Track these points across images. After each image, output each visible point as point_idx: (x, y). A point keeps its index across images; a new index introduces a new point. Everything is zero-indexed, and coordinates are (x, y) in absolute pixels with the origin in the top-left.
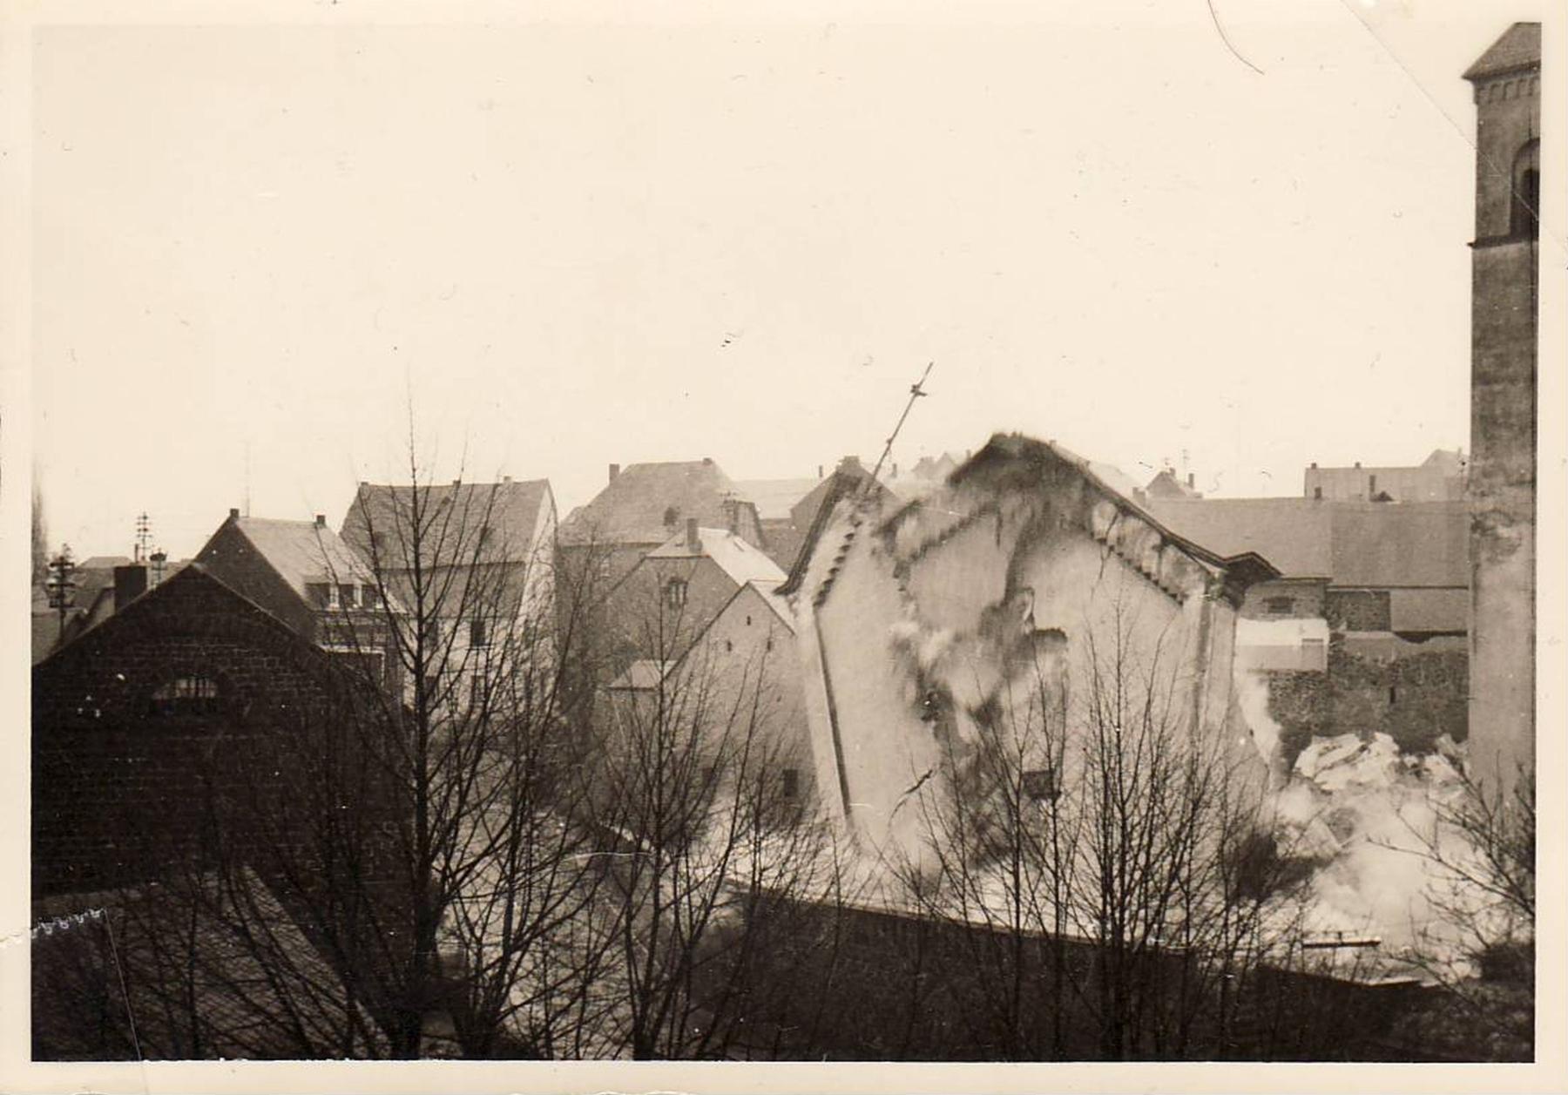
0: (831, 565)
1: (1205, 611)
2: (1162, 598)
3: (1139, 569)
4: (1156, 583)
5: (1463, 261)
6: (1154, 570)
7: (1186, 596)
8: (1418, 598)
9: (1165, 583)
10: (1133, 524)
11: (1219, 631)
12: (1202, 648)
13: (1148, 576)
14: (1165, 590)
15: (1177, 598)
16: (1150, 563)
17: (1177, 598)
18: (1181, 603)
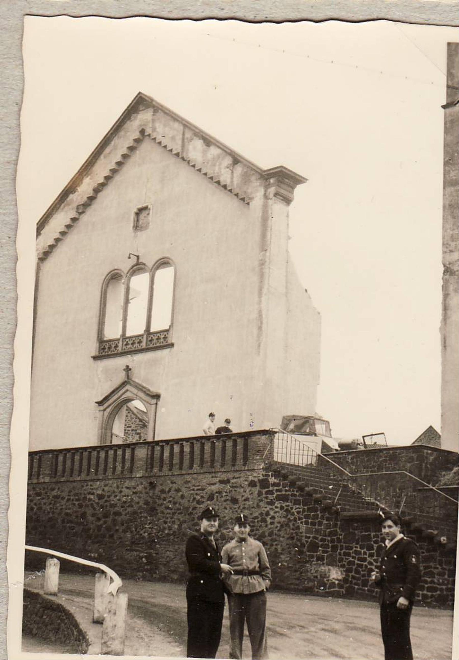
0: (57, 235)
1: (265, 207)
2: (235, 202)
3: (218, 183)
4: (230, 191)
5: (438, 117)
6: (228, 182)
7: (251, 199)
8: (363, 623)
9: (236, 191)
10: (214, 151)
11: (276, 222)
12: (264, 235)
13: (225, 187)
14: (237, 195)
15: (245, 201)
16: (225, 178)
17: (245, 201)
18: (248, 204)
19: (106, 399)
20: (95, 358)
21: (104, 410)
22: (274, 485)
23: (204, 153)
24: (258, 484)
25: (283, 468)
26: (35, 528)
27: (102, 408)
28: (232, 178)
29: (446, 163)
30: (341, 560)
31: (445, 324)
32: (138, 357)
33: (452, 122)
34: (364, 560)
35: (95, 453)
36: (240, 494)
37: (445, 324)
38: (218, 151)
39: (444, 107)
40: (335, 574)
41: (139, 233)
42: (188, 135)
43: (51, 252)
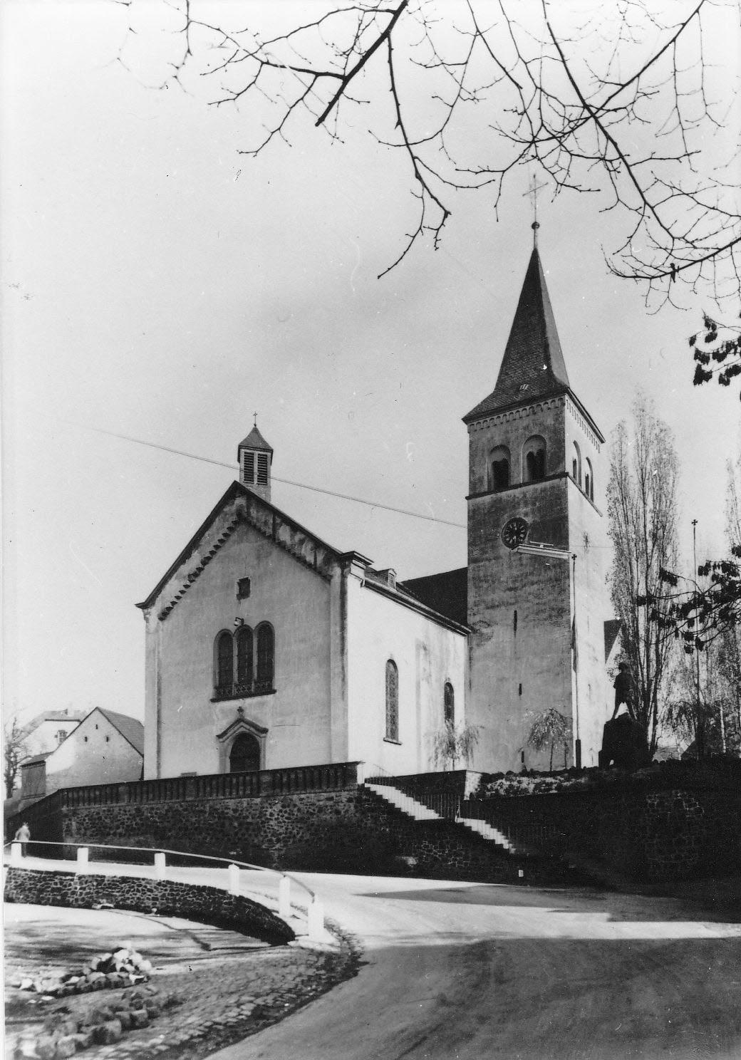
10: (299, 536)
16: (310, 558)
17: (327, 579)
19: (225, 733)
20: (213, 701)
21: (224, 742)
22: (366, 800)
23: (292, 537)
24: (354, 800)
25: (610, 943)
26: (291, 866)
27: (221, 740)
28: (315, 559)
29: (469, 544)
30: (415, 852)
31: (471, 670)
32: (248, 701)
33: (474, 511)
34: (431, 851)
35: (228, 779)
36: (341, 807)
37: (471, 670)
38: (303, 536)
39: (467, 498)
40: (411, 861)
41: (242, 601)
42: (278, 521)
43: (168, 614)
